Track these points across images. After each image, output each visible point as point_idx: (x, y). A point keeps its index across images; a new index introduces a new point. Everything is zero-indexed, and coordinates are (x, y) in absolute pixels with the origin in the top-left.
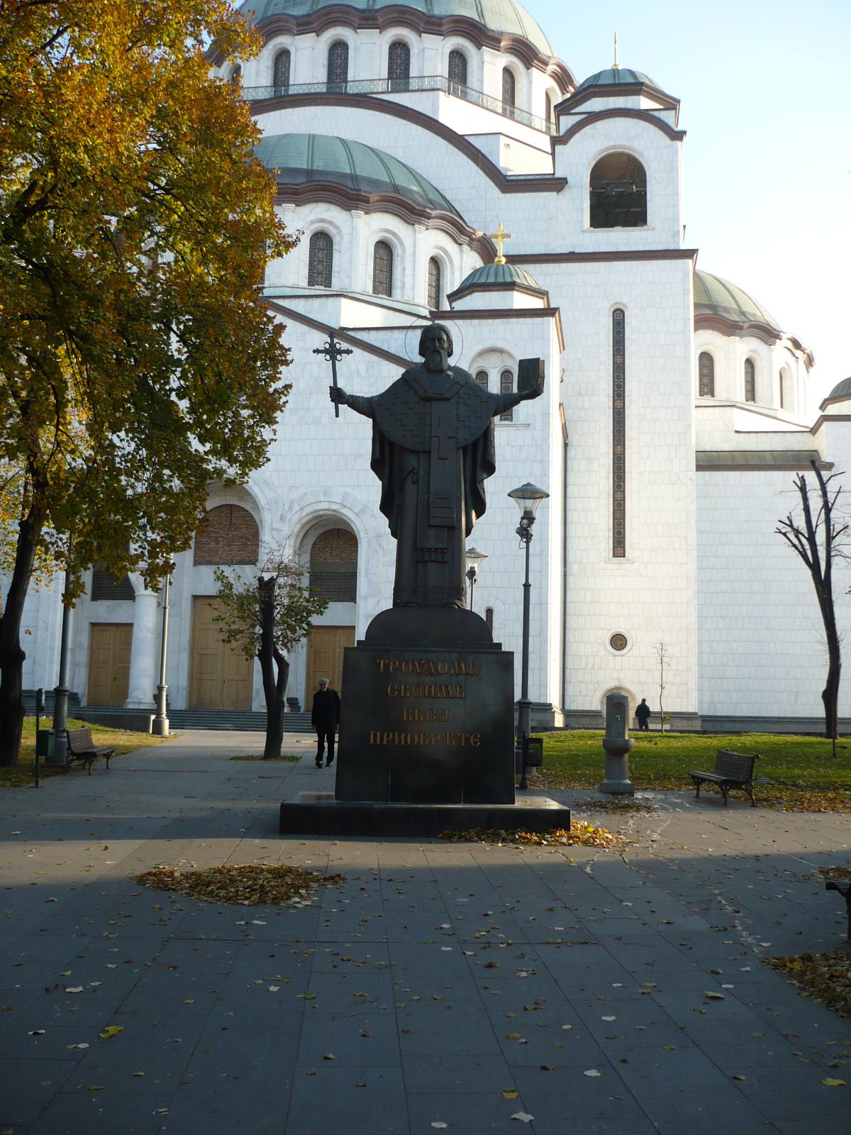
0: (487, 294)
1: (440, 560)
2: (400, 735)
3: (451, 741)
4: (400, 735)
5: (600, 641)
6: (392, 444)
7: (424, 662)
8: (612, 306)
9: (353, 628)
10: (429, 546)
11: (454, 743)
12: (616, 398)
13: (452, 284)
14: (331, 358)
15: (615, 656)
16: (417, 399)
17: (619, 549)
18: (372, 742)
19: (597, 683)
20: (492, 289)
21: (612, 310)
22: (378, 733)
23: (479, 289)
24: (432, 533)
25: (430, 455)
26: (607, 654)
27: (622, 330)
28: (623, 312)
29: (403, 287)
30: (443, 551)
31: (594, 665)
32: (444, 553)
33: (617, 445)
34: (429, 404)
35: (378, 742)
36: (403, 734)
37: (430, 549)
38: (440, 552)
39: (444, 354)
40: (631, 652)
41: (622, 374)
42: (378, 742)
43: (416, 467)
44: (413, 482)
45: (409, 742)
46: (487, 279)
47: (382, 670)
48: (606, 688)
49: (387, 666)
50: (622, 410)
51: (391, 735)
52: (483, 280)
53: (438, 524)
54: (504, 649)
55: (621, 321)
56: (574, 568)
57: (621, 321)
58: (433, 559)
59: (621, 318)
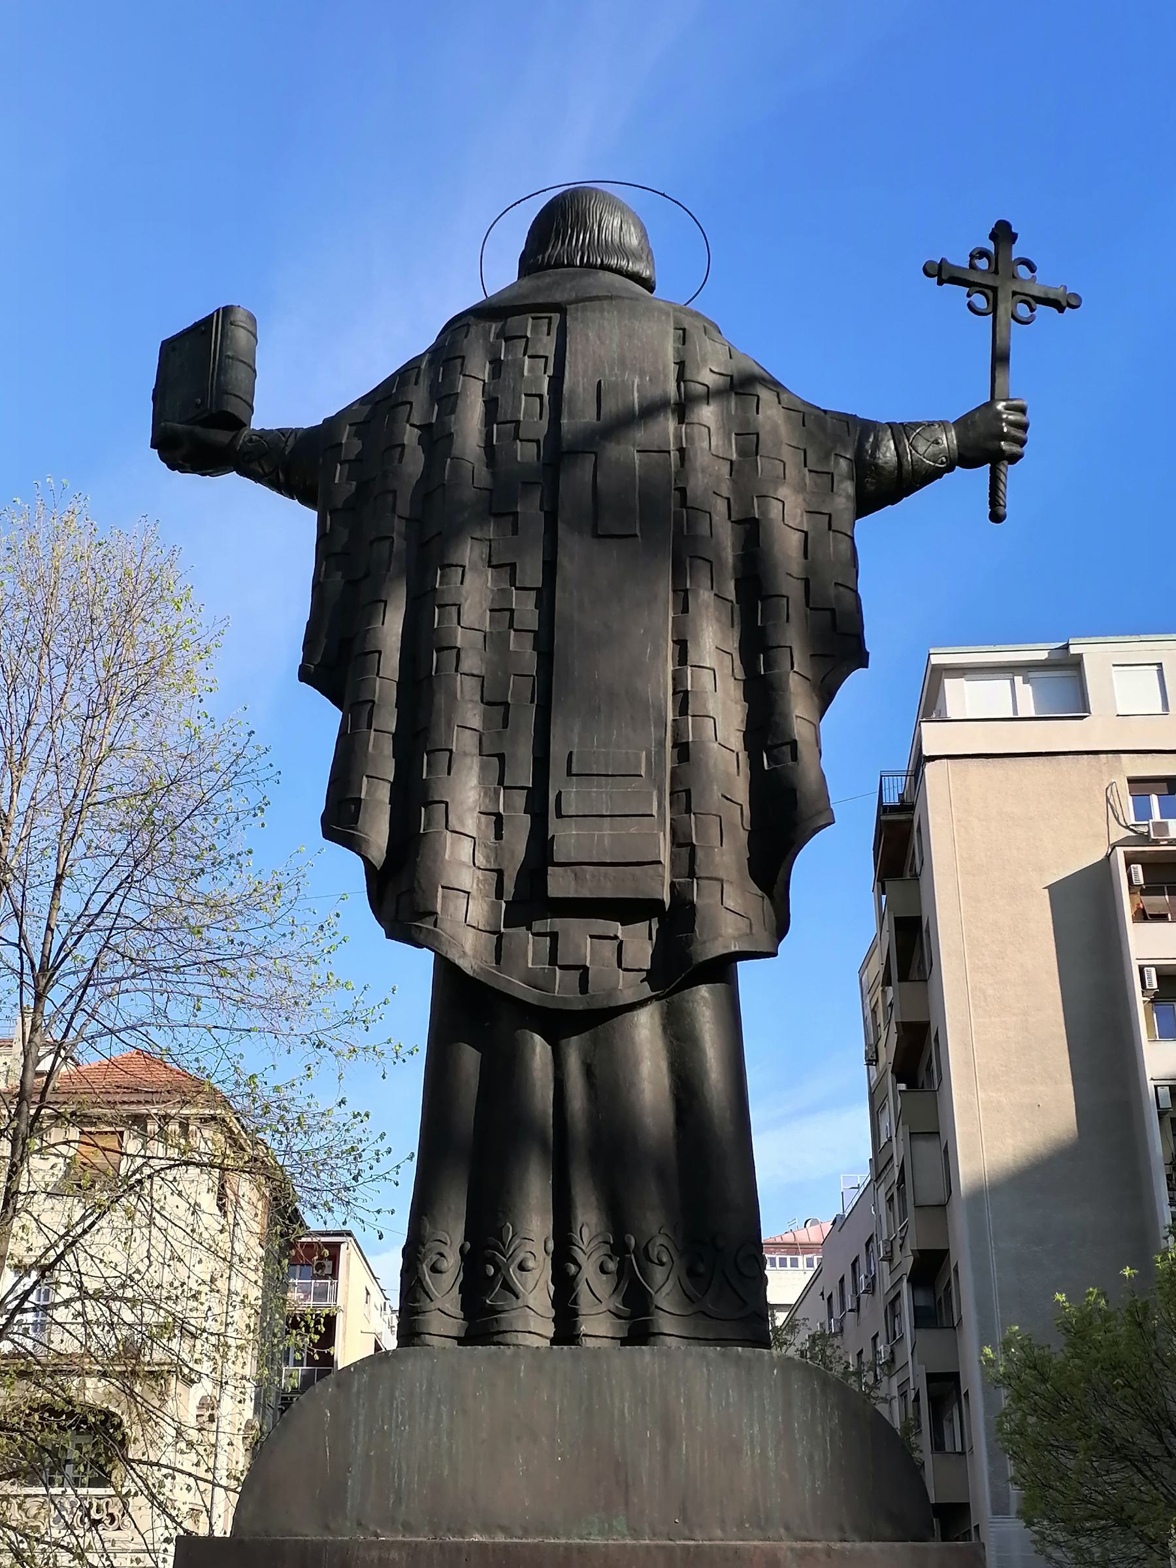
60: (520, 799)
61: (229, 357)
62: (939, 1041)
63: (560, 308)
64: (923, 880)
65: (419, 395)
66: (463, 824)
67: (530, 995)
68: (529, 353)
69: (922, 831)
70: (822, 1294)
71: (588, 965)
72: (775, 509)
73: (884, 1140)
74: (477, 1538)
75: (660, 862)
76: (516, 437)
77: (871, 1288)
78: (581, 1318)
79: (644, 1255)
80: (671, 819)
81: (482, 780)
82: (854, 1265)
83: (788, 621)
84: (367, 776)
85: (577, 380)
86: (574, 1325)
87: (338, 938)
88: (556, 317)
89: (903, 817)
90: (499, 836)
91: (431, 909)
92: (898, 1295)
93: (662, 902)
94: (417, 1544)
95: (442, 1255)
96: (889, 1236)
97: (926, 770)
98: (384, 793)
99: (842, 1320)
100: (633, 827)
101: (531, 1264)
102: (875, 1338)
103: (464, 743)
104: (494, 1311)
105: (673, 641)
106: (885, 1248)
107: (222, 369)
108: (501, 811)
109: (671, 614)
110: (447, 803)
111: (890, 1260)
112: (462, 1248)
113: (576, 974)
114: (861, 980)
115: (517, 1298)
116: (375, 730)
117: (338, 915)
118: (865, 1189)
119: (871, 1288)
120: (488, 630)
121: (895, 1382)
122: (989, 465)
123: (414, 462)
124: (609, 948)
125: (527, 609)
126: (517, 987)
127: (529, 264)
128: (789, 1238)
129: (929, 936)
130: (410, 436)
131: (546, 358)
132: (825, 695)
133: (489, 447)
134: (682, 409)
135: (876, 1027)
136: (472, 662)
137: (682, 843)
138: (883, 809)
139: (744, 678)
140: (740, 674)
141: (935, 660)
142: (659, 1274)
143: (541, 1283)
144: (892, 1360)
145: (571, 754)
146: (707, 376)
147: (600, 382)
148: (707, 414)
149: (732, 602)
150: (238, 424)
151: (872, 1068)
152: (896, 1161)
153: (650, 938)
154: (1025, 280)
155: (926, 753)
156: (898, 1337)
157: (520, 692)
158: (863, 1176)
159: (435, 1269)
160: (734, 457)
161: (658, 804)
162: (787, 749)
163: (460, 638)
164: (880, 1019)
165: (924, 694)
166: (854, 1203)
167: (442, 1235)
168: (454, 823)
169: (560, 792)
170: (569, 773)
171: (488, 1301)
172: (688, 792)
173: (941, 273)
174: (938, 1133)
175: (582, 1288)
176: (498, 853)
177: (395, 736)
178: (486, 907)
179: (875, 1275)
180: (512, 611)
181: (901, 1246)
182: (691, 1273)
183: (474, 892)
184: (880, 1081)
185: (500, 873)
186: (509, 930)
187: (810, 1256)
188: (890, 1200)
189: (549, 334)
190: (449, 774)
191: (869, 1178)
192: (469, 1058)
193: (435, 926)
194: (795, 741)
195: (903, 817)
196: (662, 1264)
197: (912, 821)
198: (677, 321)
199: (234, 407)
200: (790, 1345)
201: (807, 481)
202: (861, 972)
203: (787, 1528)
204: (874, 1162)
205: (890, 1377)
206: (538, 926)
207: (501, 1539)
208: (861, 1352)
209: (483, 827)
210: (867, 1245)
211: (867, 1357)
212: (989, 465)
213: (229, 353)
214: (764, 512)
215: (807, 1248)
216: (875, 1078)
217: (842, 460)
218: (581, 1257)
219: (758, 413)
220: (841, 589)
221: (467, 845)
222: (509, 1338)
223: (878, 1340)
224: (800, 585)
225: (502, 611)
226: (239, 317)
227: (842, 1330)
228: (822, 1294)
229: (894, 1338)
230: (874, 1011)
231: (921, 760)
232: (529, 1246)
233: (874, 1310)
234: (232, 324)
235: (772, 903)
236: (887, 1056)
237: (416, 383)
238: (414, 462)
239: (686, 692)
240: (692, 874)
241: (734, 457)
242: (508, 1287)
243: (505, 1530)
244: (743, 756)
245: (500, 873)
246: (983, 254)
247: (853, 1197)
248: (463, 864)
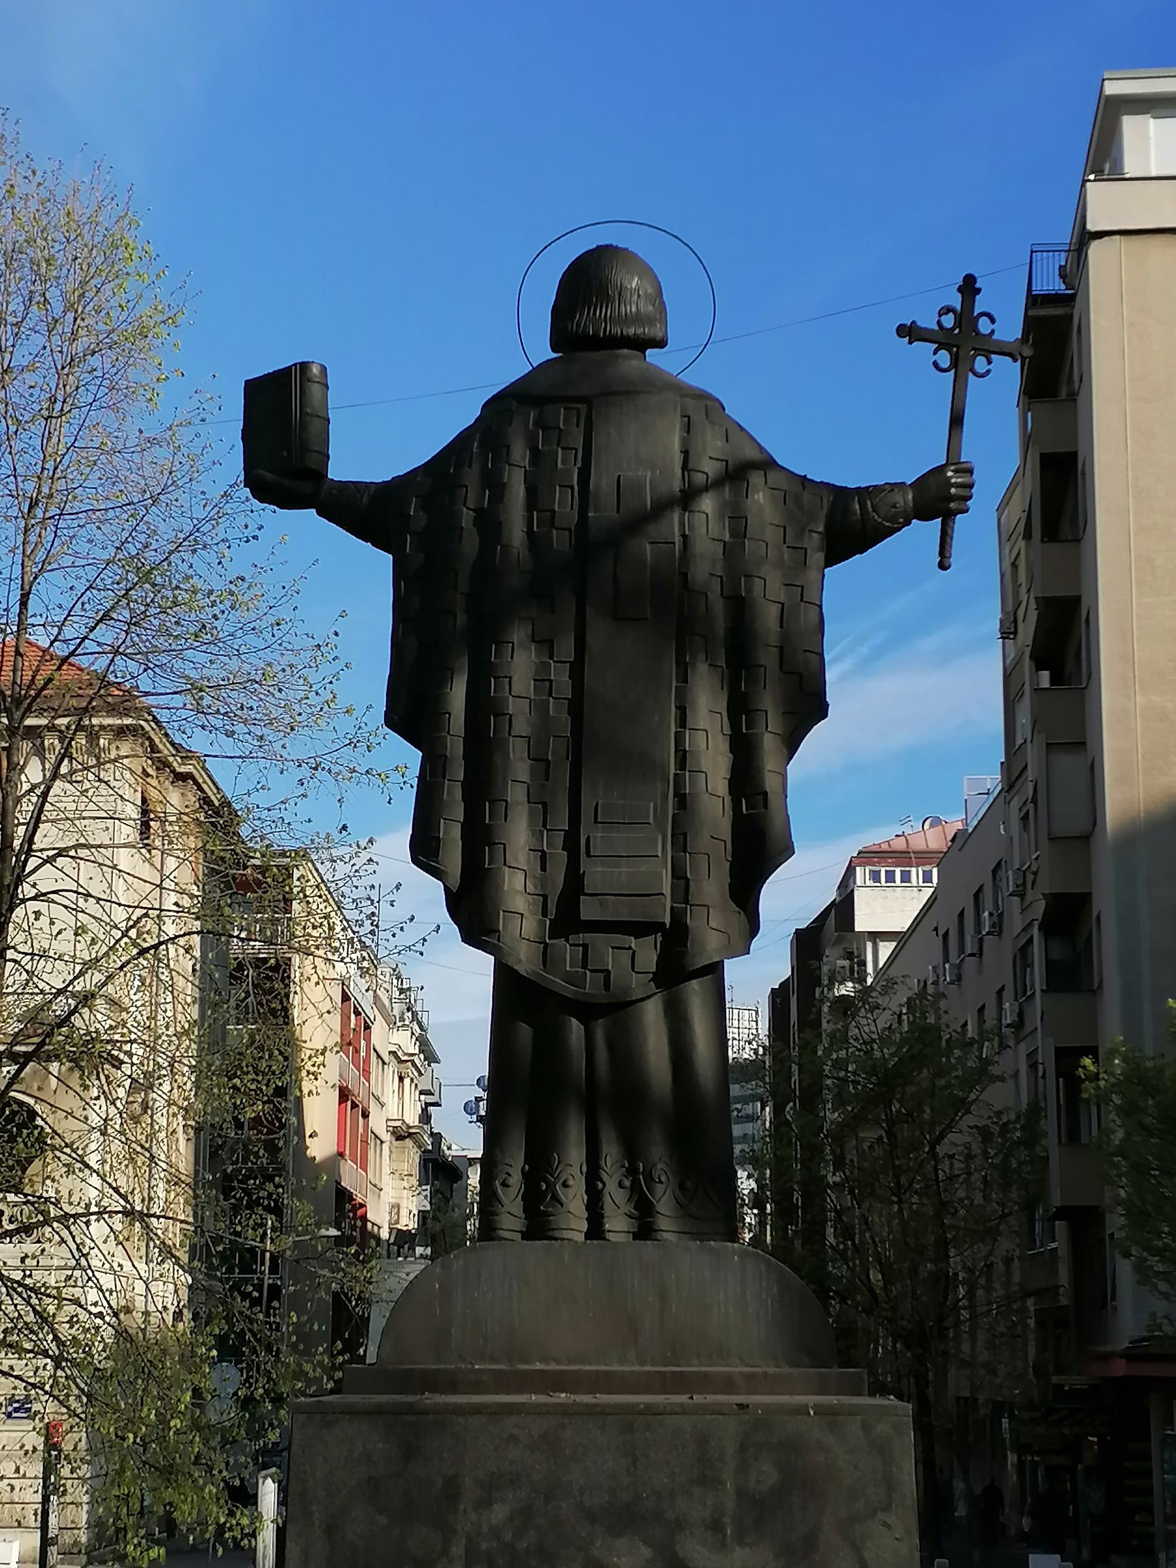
14: (955, 363)
60: (559, 839)
61: (308, 413)
62: (1091, 621)
63: (586, 400)
64: (1081, 400)
65: (471, 477)
66: (517, 861)
67: (568, 990)
68: (561, 445)
69: (1083, 331)
70: (936, 929)
71: (610, 968)
72: (758, 584)
73: (1019, 741)
74: (539, 1366)
75: (663, 894)
76: (553, 526)
77: (998, 928)
78: (605, 1220)
79: (649, 1178)
80: (672, 857)
81: (531, 822)
82: (977, 896)
83: (765, 688)
84: (444, 819)
85: (602, 482)
86: (602, 1224)
87: (339, 664)
88: (583, 407)
89: (1059, 311)
90: (543, 869)
91: (495, 928)
92: (1030, 941)
93: (664, 924)
94: (499, 1370)
95: (510, 1175)
96: (1022, 864)
97: (1090, 252)
98: (456, 832)
99: (959, 966)
100: (644, 866)
101: (571, 1182)
102: (1000, 992)
103: (516, 794)
104: (547, 1214)
105: (676, 707)
106: (1015, 879)
107: (303, 426)
108: (545, 849)
109: (674, 684)
110: (504, 845)
111: (1022, 896)
112: (523, 1168)
113: (602, 975)
114: (999, 520)
115: (562, 1205)
116: (448, 780)
117: (336, 634)
118: (995, 799)
119: (998, 928)
120: (533, 697)
121: (1023, 1049)
122: (940, 519)
123: (470, 543)
124: (625, 956)
125: (561, 677)
126: (558, 983)
127: (561, 337)
128: (900, 844)
129: (1084, 479)
130: (467, 518)
131: (576, 450)
132: (792, 744)
133: (530, 532)
134: (687, 498)
135: (1017, 586)
136: (521, 726)
137: (679, 875)
138: (1033, 300)
139: (730, 733)
140: (727, 730)
141: (1111, 88)
142: (660, 1189)
143: (579, 1196)
144: (1018, 1025)
145: (597, 804)
146: (709, 468)
147: (619, 476)
148: (707, 504)
149: (722, 667)
150: (319, 475)
151: (1009, 642)
152: (1030, 774)
153: (656, 948)
154: (985, 335)
155: (1091, 226)
156: (1029, 993)
157: (556, 750)
158: (993, 780)
159: (504, 1184)
160: (727, 538)
161: (662, 848)
162: (760, 797)
163: (512, 706)
164: (1022, 578)
165: (1097, 126)
166: (980, 816)
167: (509, 1161)
168: (510, 860)
169: (589, 837)
170: (596, 821)
171: (542, 1208)
172: (685, 835)
173: (910, 332)
174: (1084, 744)
175: (607, 1199)
176: (543, 882)
177: (463, 783)
178: (535, 923)
179: (1002, 913)
180: (551, 681)
181: (1033, 884)
182: (682, 1187)
183: (526, 913)
184: (1018, 662)
185: (545, 897)
186: (552, 941)
187: (927, 868)
188: (1025, 818)
189: (578, 426)
190: (506, 820)
191: (999, 788)
192: (525, 1031)
193: (499, 940)
194: (766, 792)
195: (1059, 311)
196: (661, 1182)
197: (1072, 315)
198: (683, 409)
199: (312, 462)
200: (884, 1009)
201: (786, 557)
202: (1000, 509)
203: (741, 1359)
204: (1006, 767)
205: (1018, 1042)
206: (573, 938)
207: (553, 1367)
208: (983, 1007)
209: (532, 861)
210: (995, 872)
211: (990, 1014)
212: (940, 519)
213: (308, 410)
214: (749, 590)
215: (922, 857)
216: (1012, 656)
217: (814, 535)
218: (605, 1177)
219: (747, 497)
220: (808, 654)
221: (520, 876)
222: (557, 1234)
223: (1004, 994)
224: (775, 651)
225: (543, 682)
226: (315, 370)
227: (959, 978)
228: (936, 929)
229: (1022, 992)
230: (1014, 565)
231: (1085, 237)
232: (570, 1170)
233: (999, 955)
234: (309, 380)
235: (746, 916)
236: (1027, 631)
237: (470, 467)
238: (470, 543)
239: (685, 751)
240: (686, 902)
241: (727, 538)
242: (556, 1199)
243: (558, 1362)
244: (728, 799)
245: (545, 897)
246: (948, 310)
247: (980, 807)
248: (518, 892)
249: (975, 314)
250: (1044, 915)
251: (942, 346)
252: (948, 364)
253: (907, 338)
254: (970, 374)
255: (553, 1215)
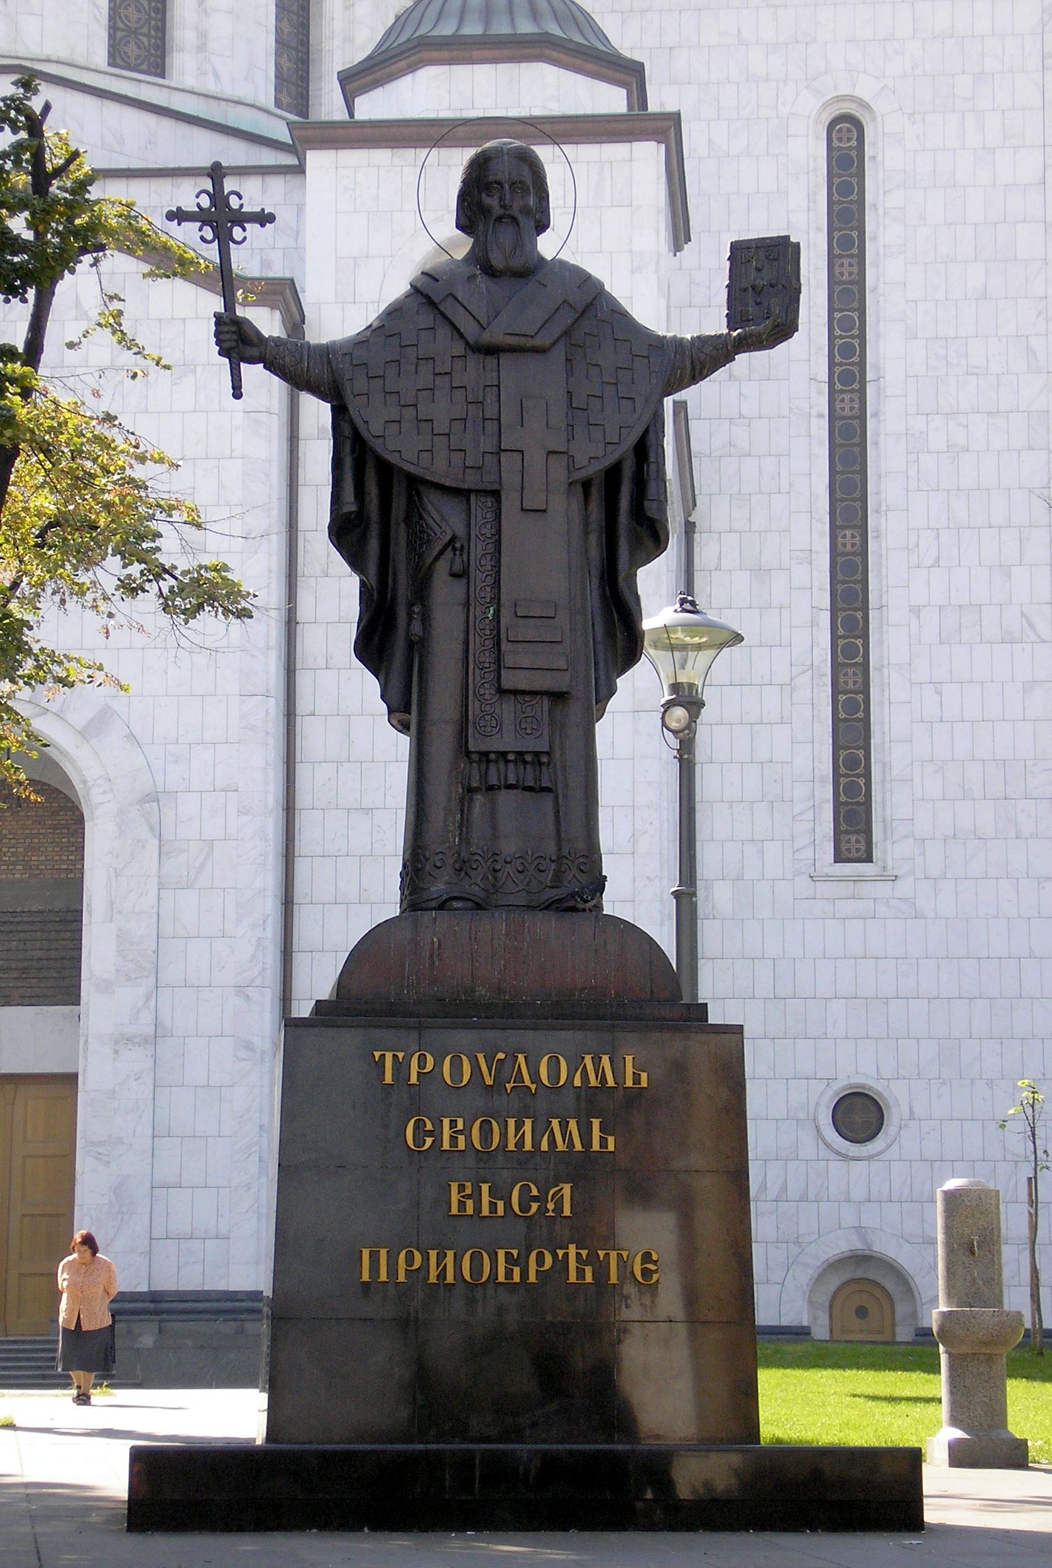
0: (461, 71)
1: (530, 783)
2: (441, 1257)
3: (581, 1273)
4: (441, 1257)
5: (802, 1115)
6: (386, 470)
7: (501, 1056)
8: (825, 106)
9: (70, 1080)
10: (495, 744)
11: (589, 1278)
12: (838, 386)
13: (349, 39)
14: (217, 236)
15: (846, 1158)
16: (459, 349)
17: (853, 838)
18: (366, 1277)
19: (797, 1243)
20: (476, 54)
21: (826, 119)
22: (383, 1253)
23: (436, 55)
24: (507, 710)
25: (499, 502)
26: (824, 1152)
27: (854, 181)
28: (858, 125)
29: (202, 48)
30: (538, 759)
31: (784, 1187)
32: (540, 764)
33: (844, 527)
34: (491, 361)
35: (383, 1277)
36: (450, 1254)
37: (503, 755)
38: (532, 763)
39: (527, 224)
40: (896, 1146)
41: (855, 315)
42: (383, 1277)
43: (460, 530)
44: (454, 575)
45: (467, 1276)
46: (460, 25)
47: (388, 1079)
48: (824, 1258)
49: (401, 1068)
50: (856, 423)
51: (418, 1256)
52: (447, 29)
53: (523, 685)
54: (715, 1017)
55: (854, 153)
56: (514, 671)
57: (854, 153)
58: (512, 780)
59: (854, 143)
249: (226, 193)
250: (866, 386)
251: (204, 223)
252: (209, 204)
253: (176, 221)
254: (231, 243)
255: (422, 303)
